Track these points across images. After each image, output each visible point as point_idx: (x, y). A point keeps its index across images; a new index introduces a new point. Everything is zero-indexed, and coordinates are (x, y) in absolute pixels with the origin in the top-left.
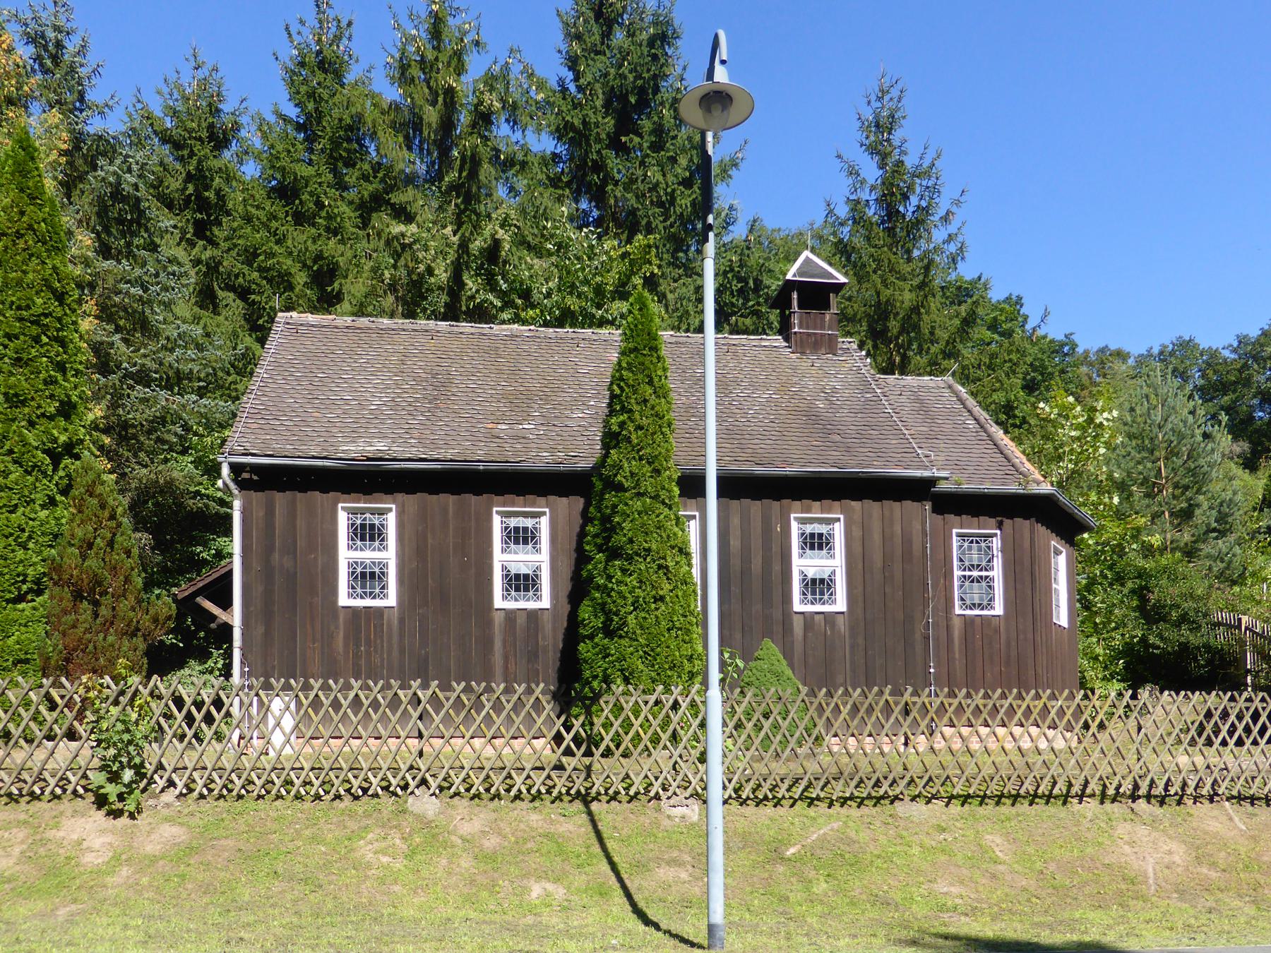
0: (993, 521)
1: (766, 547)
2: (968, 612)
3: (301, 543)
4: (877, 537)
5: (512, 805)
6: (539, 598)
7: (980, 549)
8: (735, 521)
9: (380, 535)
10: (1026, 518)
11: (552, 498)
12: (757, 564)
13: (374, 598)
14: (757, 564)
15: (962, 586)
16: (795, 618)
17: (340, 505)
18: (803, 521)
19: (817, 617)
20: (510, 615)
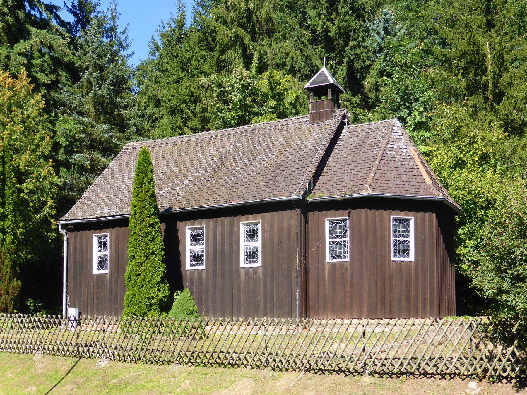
0: (346, 212)
1: (231, 238)
2: (334, 260)
3: (84, 251)
4: (276, 229)
5: (378, 379)
6: (409, 257)
7: (340, 227)
8: (219, 227)
9: (256, 234)
10: (363, 208)
11: (110, 229)
12: (227, 246)
13: (341, 258)
14: (227, 246)
15: (395, 245)
16: (326, 264)
17: (241, 223)
18: (192, 229)
19: (250, 269)
20: (247, 270)
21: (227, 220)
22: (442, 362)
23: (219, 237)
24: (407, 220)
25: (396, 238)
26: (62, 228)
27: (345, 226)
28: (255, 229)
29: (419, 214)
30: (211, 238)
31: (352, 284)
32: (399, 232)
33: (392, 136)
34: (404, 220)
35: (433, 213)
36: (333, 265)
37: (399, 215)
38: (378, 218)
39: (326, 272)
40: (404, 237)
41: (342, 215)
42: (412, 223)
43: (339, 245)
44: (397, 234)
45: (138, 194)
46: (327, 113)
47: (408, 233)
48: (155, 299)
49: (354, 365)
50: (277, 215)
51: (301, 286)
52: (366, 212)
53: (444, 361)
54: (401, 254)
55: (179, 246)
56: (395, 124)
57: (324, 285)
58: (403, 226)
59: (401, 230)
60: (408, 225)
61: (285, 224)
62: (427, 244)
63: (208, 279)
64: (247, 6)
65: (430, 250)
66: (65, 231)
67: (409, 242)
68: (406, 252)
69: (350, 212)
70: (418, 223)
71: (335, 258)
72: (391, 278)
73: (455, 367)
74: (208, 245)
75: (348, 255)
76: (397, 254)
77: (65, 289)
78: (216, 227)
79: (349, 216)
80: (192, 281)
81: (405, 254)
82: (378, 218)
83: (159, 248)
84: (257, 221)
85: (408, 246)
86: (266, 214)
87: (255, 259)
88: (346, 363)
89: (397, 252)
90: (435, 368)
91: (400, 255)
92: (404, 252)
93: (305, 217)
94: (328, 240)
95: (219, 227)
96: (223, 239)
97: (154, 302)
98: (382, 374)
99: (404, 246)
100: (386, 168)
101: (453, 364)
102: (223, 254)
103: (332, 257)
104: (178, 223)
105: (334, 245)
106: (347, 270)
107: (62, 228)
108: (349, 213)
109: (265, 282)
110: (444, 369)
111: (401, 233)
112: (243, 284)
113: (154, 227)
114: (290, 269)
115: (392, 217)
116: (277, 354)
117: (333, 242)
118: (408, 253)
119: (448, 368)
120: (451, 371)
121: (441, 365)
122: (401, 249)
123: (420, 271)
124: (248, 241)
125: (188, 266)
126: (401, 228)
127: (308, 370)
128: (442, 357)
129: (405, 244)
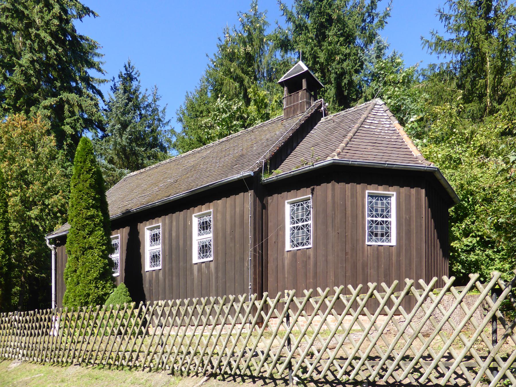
0: (309, 190)
1: (185, 233)
2: (296, 248)
6: (389, 241)
13: (303, 245)
16: (286, 253)
21: (181, 215)
22: (429, 364)
23: (174, 234)
24: (387, 197)
25: (372, 219)
26: (50, 243)
27: (308, 206)
28: (208, 220)
29: (404, 190)
30: (167, 236)
31: (315, 273)
32: (376, 210)
33: (372, 113)
34: (383, 197)
35: (422, 188)
36: (294, 254)
37: (377, 190)
38: (348, 193)
39: (286, 262)
40: (383, 217)
41: (305, 194)
42: (393, 201)
43: (301, 231)
44: (374, 213)
45: (76, 185)
46: (301, 106)
47: (388, 212)
48: (91, 297)
49: (271, 367)
50: (229, 201)
51: (255, 279)
52: (333, 186)
53: (433, 364)
54: (379, 237)
55: (140, 249)
56: (378, 103)
57: (284, 278)
58: (382, 204)
59: (379, 209)
60: (388, 203)
61: (238, 210)
62: (413, 226)
63: (165, 279)
64: (245, 50)
65: (416, 233)
66: (53, 246)
67: (390, 223)
68: (386, 234)
69: (313, 189)
70: (401, 200)
71: (297, 246)
72: (365, 266)
73: (455, 373)
74: (164, 243)
75: (311, 241)
76: (374, 237)
77: (53, 299)
78: (171, 223)
79: (312, 194)
80: (150, 282)
81: (384, 238)
82: (348, 193)
83: (98, 243)
84: (208, 211)
85: (388, 228)
86: (218, 201)
87: (208, 254)
88: (260, 364)
89: (373, 234)
90: (416, 375)
91: (378, 239)
92: (382, 235)
93: (261, 200)
94: (288, 226)
95: (174, 223)
96: (178, 236)
97: (90, 300)
98: (321, 383)
99: (382, 228)
100: (362, 140)
101: (452, 368)
102: (177, 251)
103: (293, 245)
104: (139, 224)
105: (296, 231)
106: (309, 258)
107: (50, 243)
108: (313, 190)
109: (217, 278)
110: (432, 377)
111: (380, 213)
112: (196, 281)
113: (94, 221)
114: (242, 260)
115: (367, 191)
116: (233, 354)
117: (294, 227)
118: (388, 236)
119: (442, 375)
120: (448, 381)
121: (428, 370)
122: (379, 231)
123: (403, 258)
124: (199, 232)
125: (147, 266)
126: (379, 206)
127: (214, 375)
128: (429, 356)
129: (385, 226)
